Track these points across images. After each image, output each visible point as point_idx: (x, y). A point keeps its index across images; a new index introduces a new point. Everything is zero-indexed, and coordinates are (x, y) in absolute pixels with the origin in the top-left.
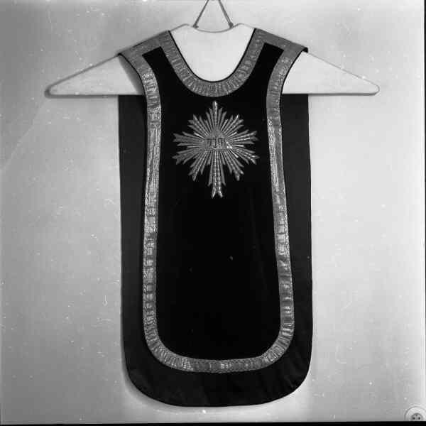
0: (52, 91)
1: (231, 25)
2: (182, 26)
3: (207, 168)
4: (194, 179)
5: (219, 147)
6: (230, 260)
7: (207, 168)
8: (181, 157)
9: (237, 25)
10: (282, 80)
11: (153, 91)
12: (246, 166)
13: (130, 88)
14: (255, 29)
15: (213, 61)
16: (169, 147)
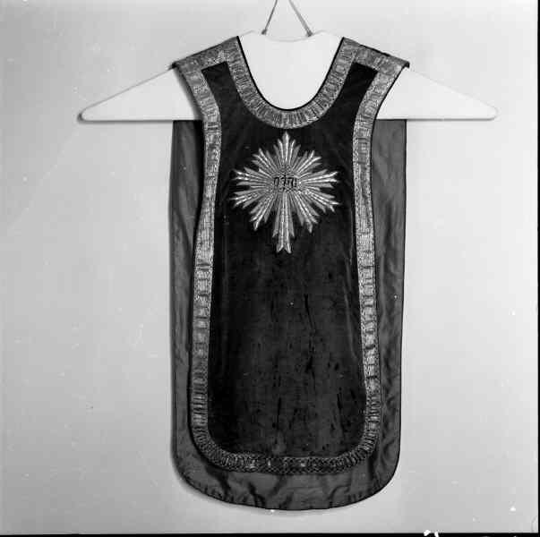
0: (85, 116)
1: (310, 34)
2: (250, 32)
3: (273, 215)
4: (289, 250)
5: (291, 192)
6: (513, 512)
7: (273, 215)
8: (242, 199)
9: (317, 33)
10: (254, 88)
11: (213, 114)
12: (323, 216)
13: (189, 115)
14: (343, 39)
15: (290, 79)
16: (228, 186)
